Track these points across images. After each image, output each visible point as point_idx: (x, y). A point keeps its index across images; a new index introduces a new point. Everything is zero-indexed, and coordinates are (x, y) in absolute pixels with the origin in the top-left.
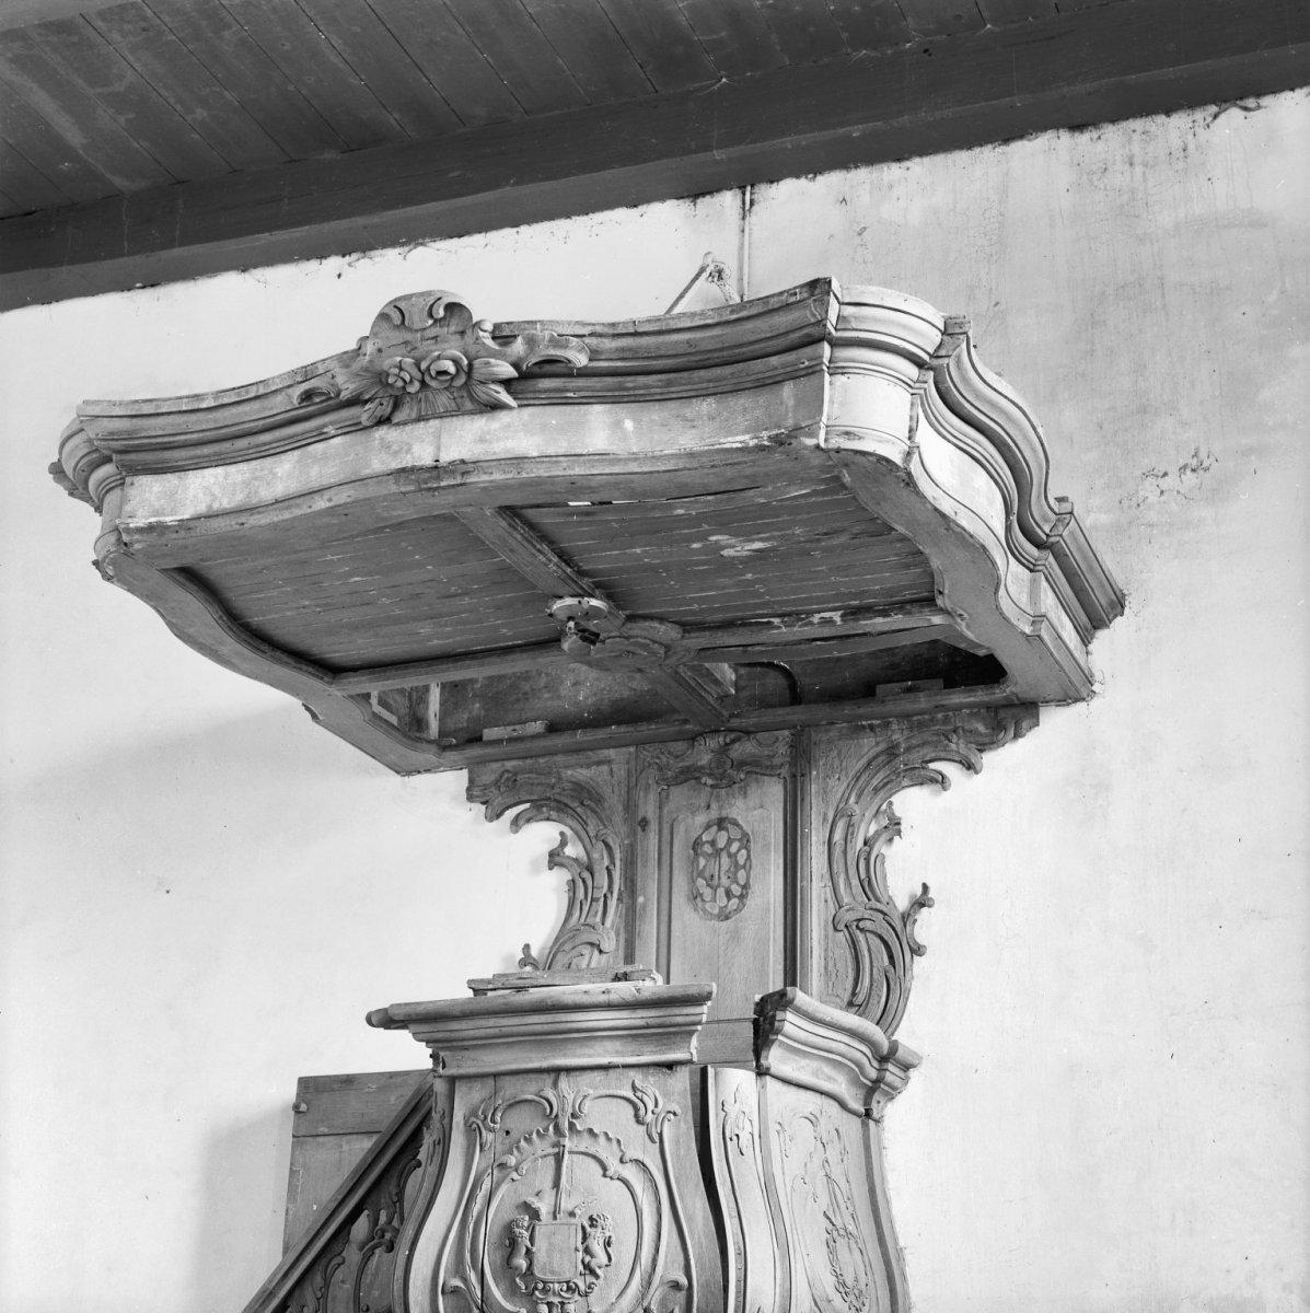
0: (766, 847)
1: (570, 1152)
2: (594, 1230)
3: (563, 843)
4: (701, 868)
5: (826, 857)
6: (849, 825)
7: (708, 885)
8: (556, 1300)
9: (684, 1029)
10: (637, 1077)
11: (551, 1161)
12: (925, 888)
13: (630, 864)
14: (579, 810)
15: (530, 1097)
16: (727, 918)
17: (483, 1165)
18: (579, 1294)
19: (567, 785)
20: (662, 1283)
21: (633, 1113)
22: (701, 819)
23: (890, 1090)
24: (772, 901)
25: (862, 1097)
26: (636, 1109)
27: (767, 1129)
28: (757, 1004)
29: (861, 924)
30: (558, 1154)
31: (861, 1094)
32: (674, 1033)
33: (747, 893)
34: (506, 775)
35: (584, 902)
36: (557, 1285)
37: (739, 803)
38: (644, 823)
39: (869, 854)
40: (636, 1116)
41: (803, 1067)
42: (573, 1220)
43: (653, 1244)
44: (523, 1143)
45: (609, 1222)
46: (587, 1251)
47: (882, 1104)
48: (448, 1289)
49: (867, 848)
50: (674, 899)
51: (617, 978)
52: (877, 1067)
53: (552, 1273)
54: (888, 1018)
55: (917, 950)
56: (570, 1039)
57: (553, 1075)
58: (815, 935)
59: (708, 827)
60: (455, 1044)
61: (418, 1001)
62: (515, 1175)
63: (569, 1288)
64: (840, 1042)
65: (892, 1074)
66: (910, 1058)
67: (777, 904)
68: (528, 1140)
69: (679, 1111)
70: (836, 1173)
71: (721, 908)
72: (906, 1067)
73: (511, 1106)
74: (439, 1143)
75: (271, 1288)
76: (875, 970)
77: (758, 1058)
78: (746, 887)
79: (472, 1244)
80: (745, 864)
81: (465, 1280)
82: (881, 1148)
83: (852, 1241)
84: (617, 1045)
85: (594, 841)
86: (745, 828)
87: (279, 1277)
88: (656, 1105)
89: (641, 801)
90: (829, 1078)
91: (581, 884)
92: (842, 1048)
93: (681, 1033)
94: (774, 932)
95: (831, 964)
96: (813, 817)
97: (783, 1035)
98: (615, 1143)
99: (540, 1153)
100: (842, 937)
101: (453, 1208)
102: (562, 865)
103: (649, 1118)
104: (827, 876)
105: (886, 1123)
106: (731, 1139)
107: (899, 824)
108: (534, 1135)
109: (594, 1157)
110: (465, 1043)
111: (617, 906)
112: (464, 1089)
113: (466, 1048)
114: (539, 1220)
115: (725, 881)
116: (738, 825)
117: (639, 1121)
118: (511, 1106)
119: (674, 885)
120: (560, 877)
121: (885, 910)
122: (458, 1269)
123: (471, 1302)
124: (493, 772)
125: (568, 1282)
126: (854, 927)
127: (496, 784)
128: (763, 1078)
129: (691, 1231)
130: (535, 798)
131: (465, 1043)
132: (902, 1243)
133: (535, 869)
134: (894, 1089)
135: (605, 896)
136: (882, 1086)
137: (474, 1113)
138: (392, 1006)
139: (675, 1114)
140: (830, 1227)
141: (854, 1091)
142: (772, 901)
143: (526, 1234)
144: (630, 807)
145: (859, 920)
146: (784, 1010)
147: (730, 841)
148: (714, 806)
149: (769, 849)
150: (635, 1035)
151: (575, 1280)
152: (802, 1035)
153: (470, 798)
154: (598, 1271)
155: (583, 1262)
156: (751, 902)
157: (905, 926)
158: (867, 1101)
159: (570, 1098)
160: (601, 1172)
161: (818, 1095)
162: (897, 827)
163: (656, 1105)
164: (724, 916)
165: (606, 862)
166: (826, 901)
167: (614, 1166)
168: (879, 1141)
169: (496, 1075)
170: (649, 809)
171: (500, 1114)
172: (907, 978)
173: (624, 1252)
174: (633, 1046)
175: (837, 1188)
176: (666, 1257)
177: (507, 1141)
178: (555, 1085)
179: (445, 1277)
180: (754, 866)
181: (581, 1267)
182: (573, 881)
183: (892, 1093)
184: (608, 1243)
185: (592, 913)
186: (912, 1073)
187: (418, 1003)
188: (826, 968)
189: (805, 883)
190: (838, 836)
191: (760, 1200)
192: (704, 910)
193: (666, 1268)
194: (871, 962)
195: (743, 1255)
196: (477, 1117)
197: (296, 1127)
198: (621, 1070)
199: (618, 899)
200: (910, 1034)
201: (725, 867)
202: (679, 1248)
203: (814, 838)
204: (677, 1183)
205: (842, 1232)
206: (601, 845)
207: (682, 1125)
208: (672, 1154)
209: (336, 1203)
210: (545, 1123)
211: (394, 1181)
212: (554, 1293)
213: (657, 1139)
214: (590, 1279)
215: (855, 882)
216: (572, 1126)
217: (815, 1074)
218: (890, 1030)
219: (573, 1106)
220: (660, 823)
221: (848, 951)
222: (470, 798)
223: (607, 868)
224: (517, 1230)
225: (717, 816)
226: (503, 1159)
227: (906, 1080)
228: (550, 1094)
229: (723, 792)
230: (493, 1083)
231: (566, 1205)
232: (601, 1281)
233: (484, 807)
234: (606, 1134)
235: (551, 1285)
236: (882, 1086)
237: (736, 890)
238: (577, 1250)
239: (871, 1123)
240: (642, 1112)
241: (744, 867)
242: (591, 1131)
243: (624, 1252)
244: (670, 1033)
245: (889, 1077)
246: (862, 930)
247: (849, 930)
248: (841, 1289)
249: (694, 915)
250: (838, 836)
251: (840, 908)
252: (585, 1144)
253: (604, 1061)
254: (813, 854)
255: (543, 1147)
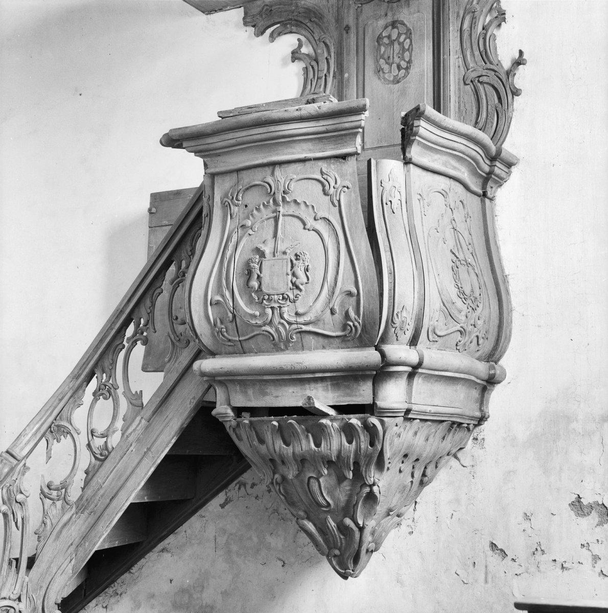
0: (422, 36)
1: (284, 215)
2: (298, 261)
3: (300, 46)
4: (382, 52)
5: (459, 39)
6: (473, 18)
7: (387, 63)
8: (276, 305)
9: (351, 131)
10: (323, 165)
11: (272, 221)
12: (521, 52)
13: (339, 55)
14: (308, 24)
15: (257, 183)
16: (398, 82)
17: (233, 227)
18: (290, 301)
19: (301, 10)
20: (341, 293)
21: (321, 188)
22: (381, 23)
23: (498, 179)
24: (426, 70)
25: (481, 184)
26: (323, 186)
27: (411, 198)
28: (403, 118)
29: (481, 79)
30: (276, 216)
31: (479, 182)
32: (345, 135)
33: (410, 66)
34: (265, 8)
35: (313, 80)
36: (276, 296)
37: (405, 11)
38: (347, 28)
39: (486, 35)
40: (324, 190)
41: (436, 160)
42: (285, 257)
43: (335, 269)
44: (255, 212)
45: (308, 256)
46: (294, 275)
47: (494, 189)
48: (214, 302)
49: (484, 31)
50: (366, 73)
51: (308, 102)
52: (489, 164)
53: (273, 289)
54: (498, 135)
55: (516, 93)
56: (279, 142)
57: (271, 168)
58: (452, 88)
59: (386, 27)
60: (211, 152)
61: (187, 126)
62: (250, 232)
63: (283, 298)
64: (460, 144)
65: (499, 169)
66: (510, 158)
67: (429, 70)
68: (258, 209)
69: (350, 186)
70: (461, 227)
71: (394, 76)
72: (509, 165)
73: (247, 189)
74: (207, 216)
75: (121, 308)
76: (489, 107)
77: (404, 154)
78: (409, 62)
79: (226, 274)
80: (409, 47)
81: (223, 296)
82: (493, 216)
83: (470, 268)
84: (309, 145)
85: (318, 42)
86: (408, 26)
87: (126, 300)
88: (336, 183)
89: (346, 15)
90: (455, 168)
91: (311, 69)
92: (462, 148)
93: (349, 134)
94: (427, 88)
95: (462, 105)
96: (450, 16)
97: (420, 137)
98: (310, 208)
99: (265, 217)
100: (469, 88)
101: (215, 255)
102: (299, 59)
103: (332, 191)
104: (460, 51)
105: (498, 200)
106: (387, 204)
107: (504, 14)
108: (262, 206)
109: (298, 217)
110: (218, 151)
111: (333, 80)
112: (220, 181)
113: (219, 155)
114: (265, 258)
115: (397, 60)
116: (404, 24)
117: (325, 193)
118: (247, 189)
119: (366, 64)
120: (298, 67)
121: (496, 69)
122: (219, 290)
123: (227, 309)
124: (259, 6)
125: (283, 294)
126: (476, 81)
127: (260, 14)
128: (408, 166)
129: (358, 260)
130: (283, 20)
131: (218, 151)
132: (507, 272)
133: (285, 64)
134: (502, 179)
135: (326, 75)
136: (493, 176)
137: (226, 196)
138: (171, 130)
139: (348, 188)
140: (455, 259)
141: (474, 180)
142: (426, 70)
143: (257, 267)
144: (339, 19)
145: (479, 77)
146: (419, 120)
147: (399, 35)
148: (390, 14)
149: (424, 39)
150: (320, 138)
151: (287, 293)
152: (434, 138)
153: (246, 24)
154: (301, 287)
155: (291, 282)
156: (412, 71)
157: (508, 78)
158: (484, 187)
159: (282, 181)
160: (302, 226)
161: (448, 179)
162: (503, 16)
163: (336, 183)
164: (397, 81)
165: (326, 55)
166: (459, 67)
167: (310, 223)
168: (492, 211)
169: (238, 171)
170: (350, 20)
171: (241, 195)
172: (510, 109)
173: (317, 275)
174: (320, 146)
175: (460, 236)
176: (343, 276)
177: (246, 211)
178: (273, 174)
179: (212, 295)
180: (414, 49)
181: (290, 285)
182: (306, 68)
183: (500, 181)
184: (307, 270)
185: (318, 86)
186: (513, 169)
187: (186, 127)
188: (459, 108)
189: (446, 56)
190: (466, 26)
191: (405, 240)
192: (384, 78)
193: (343, 283)
194: (487, 102)
195: (393, 274)
196: (228, 198)
197: (150, 221)
198: (313, 162)
199: (333, 77)
200: (511, 146)
201: (396, 51)
202: (351, 271)
203: (451, 28)
204: (350, 230)
205: (463, 262)
206: (322, 45)
207: (353, 195)
208: (346, 213)
209: (155, 258)
210: (268, 198)
211: (189, 243)
212: (275, 301)
213: (337, 204)
214: (298, 292)
215: (477, 53)
216: (284, 199)
217: (445, 164)
218: (499, 143)
219: (284, 186)
220: (357, 28)
221: (473, 97)
222: (246, 24)
223: (326, 58)
224: (252, 264)
225: (391, 20)
226: (243, 223)
227: (509, 174)
228: (270, 180)
229: (395, 4)
230: (236, 175)
231: (281, 247)
232: (303, 293)
233: (253, 29)
234: (305, 203)
235: (273, 296)
236: (493, 176)
237: (404, 64)
238: (287, 274)
239: (487, 201)
240: (327, 187)
241: (408, 50)
242: (295, 201)
243: (317, 275)
244: (342, 135)
245: (497, 171)
246: (481, 83)
247: (473, 83)
248: (462, 296)
249: (378, 82)
250: (466, 26)
251: (468, 70)
252: (292, 209)
253: (302, 156)
254: (451, 38)
255: (267, 213)
